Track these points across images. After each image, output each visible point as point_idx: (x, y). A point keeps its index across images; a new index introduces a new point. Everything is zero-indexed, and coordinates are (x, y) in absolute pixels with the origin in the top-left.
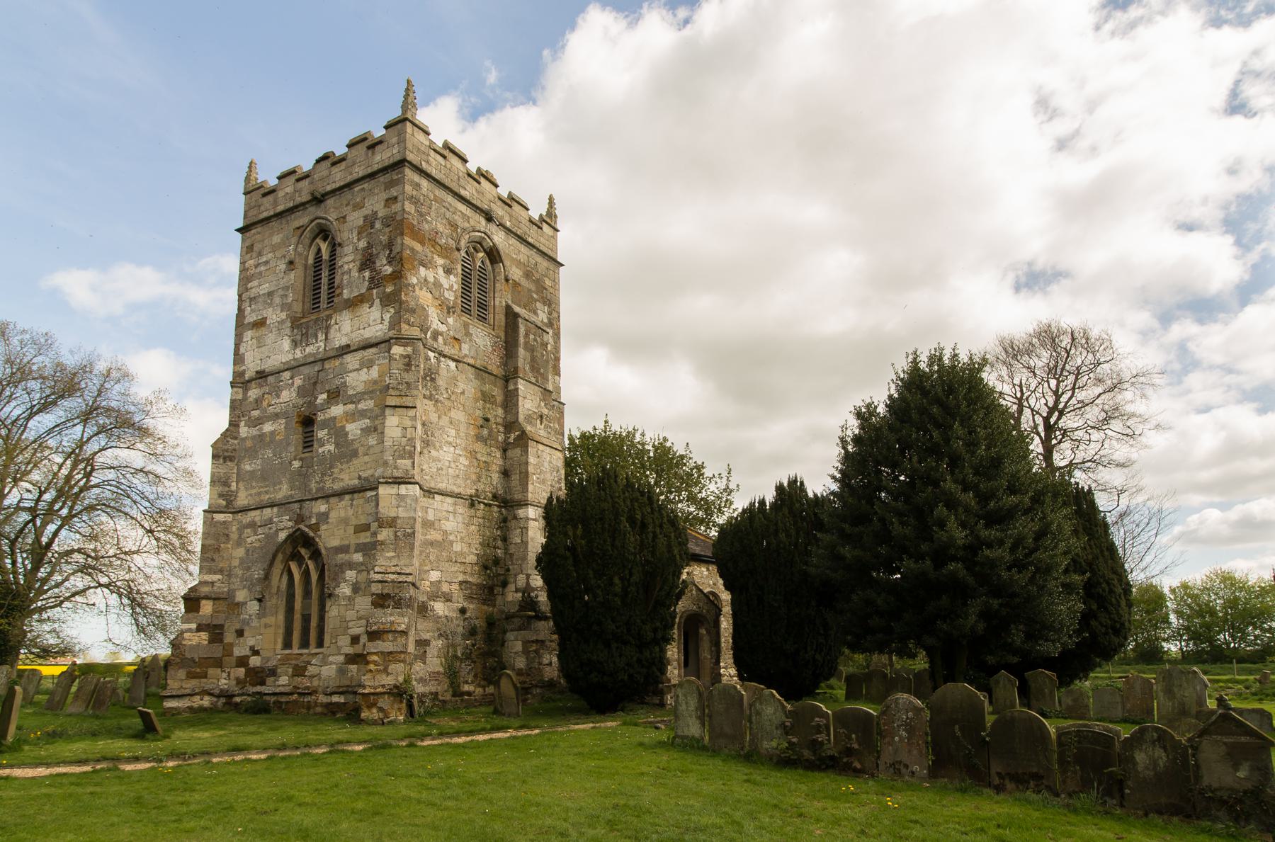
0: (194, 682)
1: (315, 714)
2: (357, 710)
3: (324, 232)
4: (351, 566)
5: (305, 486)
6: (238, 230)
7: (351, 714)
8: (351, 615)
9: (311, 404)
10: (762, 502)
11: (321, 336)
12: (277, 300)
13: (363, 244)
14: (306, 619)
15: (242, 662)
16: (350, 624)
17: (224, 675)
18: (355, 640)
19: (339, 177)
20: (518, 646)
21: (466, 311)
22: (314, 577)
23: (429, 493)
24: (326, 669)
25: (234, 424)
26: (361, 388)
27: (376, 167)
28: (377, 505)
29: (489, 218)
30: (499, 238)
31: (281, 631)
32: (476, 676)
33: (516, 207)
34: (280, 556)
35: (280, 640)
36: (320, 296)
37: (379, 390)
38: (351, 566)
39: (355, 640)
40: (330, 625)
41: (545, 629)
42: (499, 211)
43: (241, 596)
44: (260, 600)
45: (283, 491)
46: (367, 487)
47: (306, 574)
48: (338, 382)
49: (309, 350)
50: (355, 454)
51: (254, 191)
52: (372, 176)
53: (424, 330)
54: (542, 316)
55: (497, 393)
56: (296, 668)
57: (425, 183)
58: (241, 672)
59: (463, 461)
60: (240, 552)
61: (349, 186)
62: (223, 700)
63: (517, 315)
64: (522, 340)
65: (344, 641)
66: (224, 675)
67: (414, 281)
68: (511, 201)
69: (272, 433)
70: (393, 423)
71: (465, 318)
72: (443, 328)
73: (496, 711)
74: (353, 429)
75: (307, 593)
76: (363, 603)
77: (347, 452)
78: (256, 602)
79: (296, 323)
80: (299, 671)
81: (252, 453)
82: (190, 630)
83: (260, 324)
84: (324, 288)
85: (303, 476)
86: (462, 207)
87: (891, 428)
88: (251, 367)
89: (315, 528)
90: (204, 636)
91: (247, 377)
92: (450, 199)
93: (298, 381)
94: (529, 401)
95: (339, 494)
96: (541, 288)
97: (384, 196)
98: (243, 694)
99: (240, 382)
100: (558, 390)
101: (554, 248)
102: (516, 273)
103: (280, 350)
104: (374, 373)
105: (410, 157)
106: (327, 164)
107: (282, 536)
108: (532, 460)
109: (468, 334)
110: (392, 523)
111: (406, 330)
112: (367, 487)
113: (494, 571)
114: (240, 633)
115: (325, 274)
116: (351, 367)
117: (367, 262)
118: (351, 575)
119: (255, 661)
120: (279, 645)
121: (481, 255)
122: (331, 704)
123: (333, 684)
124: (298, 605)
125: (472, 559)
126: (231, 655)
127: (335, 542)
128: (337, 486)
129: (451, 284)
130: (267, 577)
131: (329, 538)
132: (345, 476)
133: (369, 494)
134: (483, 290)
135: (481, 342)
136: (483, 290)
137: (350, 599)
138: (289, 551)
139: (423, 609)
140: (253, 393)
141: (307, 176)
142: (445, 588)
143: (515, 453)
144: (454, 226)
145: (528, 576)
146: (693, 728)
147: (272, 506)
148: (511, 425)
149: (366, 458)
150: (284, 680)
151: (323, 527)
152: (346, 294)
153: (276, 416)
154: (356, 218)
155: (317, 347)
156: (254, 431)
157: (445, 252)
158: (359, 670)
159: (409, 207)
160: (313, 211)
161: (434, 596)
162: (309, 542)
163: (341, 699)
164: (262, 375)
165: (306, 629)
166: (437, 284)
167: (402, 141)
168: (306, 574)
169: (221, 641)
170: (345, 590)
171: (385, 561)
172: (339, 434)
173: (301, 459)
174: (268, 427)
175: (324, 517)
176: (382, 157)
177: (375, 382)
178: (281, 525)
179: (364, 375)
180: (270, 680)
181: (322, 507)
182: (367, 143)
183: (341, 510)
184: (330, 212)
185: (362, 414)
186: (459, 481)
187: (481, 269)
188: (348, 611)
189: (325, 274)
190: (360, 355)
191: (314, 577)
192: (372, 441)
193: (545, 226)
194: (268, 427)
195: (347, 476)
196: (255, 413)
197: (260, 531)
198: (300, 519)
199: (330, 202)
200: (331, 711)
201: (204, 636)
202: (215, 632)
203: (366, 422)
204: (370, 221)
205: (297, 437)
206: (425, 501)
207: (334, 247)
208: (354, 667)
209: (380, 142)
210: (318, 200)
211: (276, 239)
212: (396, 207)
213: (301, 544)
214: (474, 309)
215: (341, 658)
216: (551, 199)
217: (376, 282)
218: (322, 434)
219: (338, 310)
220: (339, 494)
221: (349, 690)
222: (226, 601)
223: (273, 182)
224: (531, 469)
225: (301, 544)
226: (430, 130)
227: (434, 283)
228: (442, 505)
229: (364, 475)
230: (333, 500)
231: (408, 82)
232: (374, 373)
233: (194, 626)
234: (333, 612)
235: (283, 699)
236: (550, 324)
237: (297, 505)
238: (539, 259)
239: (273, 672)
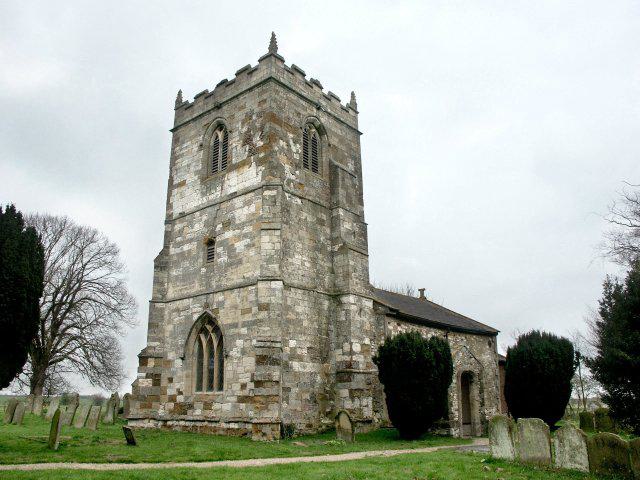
0: (145, 410)
1: (220, 435)
3: (220, 126)
4: (240, 336)
5: (208, 285)
6: (171, 131)
8: (240, 370)
9: (213, 231)
10: (598, 324)
11: (219, 188)
12: (192, 168)
13: (245, 129)
14: (211, 372)
15: (172, 399)
16: (240, 376)
17: (162, 407)
18: (244, 386)
19: (230, 93)
21: (306, 166)
22: (215, 344)
25: (166, 247)
26: (244, 219)
27: (253, 84)
28: (257, 295)
29: (319, 109)
30: (324, 119)
31: (195, 379)
33: (333, 100)
34: (194, 330)
35: (195, 385)
38: (240, 336)
39: (244, 386)
40: (227, 375)
42: (323, 103)
43: (171, 356)
44: (182, 359)
45: (197, 288)
47: (210, 342)
48: (229, 216)
49: (211, 197)
50: (240, 262)
51: (181, 106)
52: (250, 89)
53: (283, 179)
54: (351, 167)
56: (206, 404)
58: (171, 405)
59: (307, 265)
62: (160, 423)
63: (337, 167)
65: (237, 387)
66: (162, 407)
67: (276, 148)
68: (331, 97)
69: (189, 251)
72: (293, 177)
74: (240, 246)
75: (211, 355)
77: (235, 261)
78: (180, 361)
79: (203, 180)
80: (208, 406)
82: (141, 377)
83: (183, 183)
84: (220, 158)
85: (208, 277)
88: (176, 211)
89: (216, 311)
90: (150, 381)
91: (174, 217)
93: (205, 218)
95: (231, 289)
97: (258, 100)
98: (172, 420)
99: (169, 221)
101: (357, 126)
102: (334, 141)
103: (191, 199)
104: (253, 208)
107: (196, 317)
114: (171, 380)
115: (220, 150)
117: (247, 140)
118: (239, 343)
119: (180, 399)
120: (194, 389)
121: (314, 130)
122: (229, 429)
123: (230, 416)
126: (165, 394)
127: (229, 321)
128: (229, 284)
129: (297, 148)
130: (187, 343)
131: (223, 320)
132: (235, 277)
133: (250, 288)
134: (315, 153)
135: (316, 185)
137: (239, 359)
138: (199, 325)
139: (287, 367)
140: (178, 227)
141: (212, 94)
142: (299, 352)
145: (351, 344)
147: (189, 298)
149: (249, 265)
150: (198, 412)
151: (221, 311)
152: (234, 161)
153: (190, 241)
154: (240, 115)
155: (216, 195)
156: (178, 250)
157: (294, 130)
158: (247, 407)
160: (214, 114)
163: (236, 426)
164: (183, 215)
168: (210, 342)
169: (159, 385)
170: (234, 353)
172: (230, 250)
174: (186, 248)
177: (253, 214)
178: (195, 310)
179: (246, 211)
180: (189, 412)
181: (220, 297)
182: (247, 72)
183: (233, 298)
184: (225, 112)
185: (245, 236)
186: (226, 115)
187: (313, 138)
189: (220, 150)
190: (242, 198)
191: (215, 344)
192: (252, 252)
193: (351, 111)
194: (186, 248)
195: (235, 278)
196: (179, 239)
197: (182, 314)
199: (225, 108)
201: (150, 381)
202: (156, 379)
204: (249, 116)
207: (226, 138)
208: (243, 406)
209: (256, 69)
210: (218, 107)
211: (193, 133)
213: (207, 323)
215: (234, 399)
216: (353, 94)
217: (252, 152)
218: (219, 250)
219: (230, 170)
220: (231, 289)
223: (191, 101)
225: (207, 323)
226: (285, 59)
229: (246, 275)
230: (226, 293)
232: (253, 208)
233: (144, 375)
234: (228, 367)
235: (199, 424)
237: (203, 297)
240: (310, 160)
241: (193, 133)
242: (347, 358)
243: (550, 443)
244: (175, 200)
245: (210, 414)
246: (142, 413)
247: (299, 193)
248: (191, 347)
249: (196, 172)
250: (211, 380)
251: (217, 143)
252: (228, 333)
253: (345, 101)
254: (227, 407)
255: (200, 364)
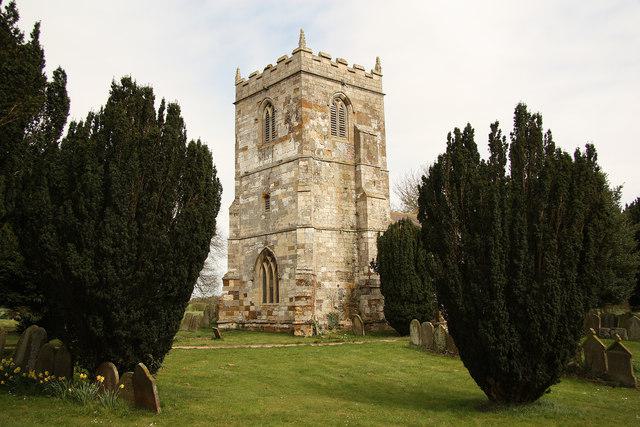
2: (294, 331)
3: (269, 104)
7: (290, 332)
8: (289, 288)
13: (285, 111)
14: (271, 289)
15: (247, 308)
18: (291, 299)
19: (275, 78)
20: (366, 303)
21: (334, 134)
23: (319, 229)
24: (280, 313)
25: (237, 198)
27: (290, 74)
29: (343, 84)
30: (349, 92)
32: (346, 317)
33: (358, 71)
36: (269, 137)
37: (295, 183)
39: (291, 299)
41: (378, 294)
42: (348, 77)
43: (245, 278)
45: (259, 230)
46: (292, 229)
50: (286, 213)
51: (241, 85)
55: (352, 174)
57: (310, 78)
60: (243, 258)
61: (279, 82)
64: (362, 144)
65: (287, 300)
70: (301, 198)
71: (334, 138)
72: (322, 147)
73: (352, 332)
74: (286, 201)
75: (271, 278)
76: (293, 282)
77: (284, 212)
79: (260, 150)
80: (270, 313)
81: (245, 211)
84: (271, 131)
86: (329, 83)
87: (422, 235)
88: (242, 171)
92: (323, 81)
94: (367, 174)
95: (281, 232)
96: (373, 111)
97: (294, 87)
100: (385, 164)
102: (358, 107)
105: (304, 68)
106: (269, 70)
107: (260, 251)
108: (369, 207)
109: (335, 147)
110: (303, 247)
111: (306, 153)
112: (292, 229)
113: (354, 263)
114: (246, 295)
115: (271, 123)
116: (283, 171)
117: (288, 120)
118: (288, 270)
119: (252, 308)
123: (283, 319)
124: (268, 283)
125: (342, 260)
127: (281, 255)
128: (281, 228)
131: (278, 253)
134: (342, 121)
135: (342, 148)
136: (342, 121)
140: (244, 183)
142: (329, 275)
143: (361, 204)
144: (325, 94)
146: (416, 340)
148: (358, 189)
150: (264, 317)
154: (282, 98)
159: (304, 93)
161: (324, 280)
162: (270, 254)
164: (247, 174)
165: (272, 294)
166: (319, 126)
167: (300, 61)
170: (285, 277)
171: (301, 263)
172: (280, 203)
173: (265, 215)
174: (251, 199)
175: (276, 242)
176: (292, 69)
181: (274, 238)
183: (283, 239)
184: (271, 95)
188: (287, 287)
189: (271, 123)
193: (375, 77)
194: (251, 199)
195: (284, 224)
198: (266, 243)
200: (283, 332)
201: (232, 296)
203: (290, 198)
204: (288, 100)
205: (263, 205)
206: (318, 234)
207: (274, 112)
210: (266, 89)
211: (250, 108)
212: (298, 93)
213: (267, 255)
214: (338, 132)
217: (292, 130)
218: (273, 203)
220: (281, 232)
221: (289, 322)
222: (240, 282)
224: (369, 212)
227: (317, 125)
228: (326, 234)
230: (279, 235)
231: (301, 31)
232: (293, 174)
234: (282, 286)
236: (379, 129)
238: (371, 95)
239: (260, 314)
240: (338, 128)
241: (250, 108)
242: (367, 277)
243: (242, 328)
244: (240, 160)
245: (272, 318)
246: (228, 318)
247: (328, 158)
248: (258, 272)
249: (255, 141)
250: (272, 295)
251: (267, 116)
252: (281, 263)
253: (369, 67)
254: (282, 313)
255: (265, 278)
